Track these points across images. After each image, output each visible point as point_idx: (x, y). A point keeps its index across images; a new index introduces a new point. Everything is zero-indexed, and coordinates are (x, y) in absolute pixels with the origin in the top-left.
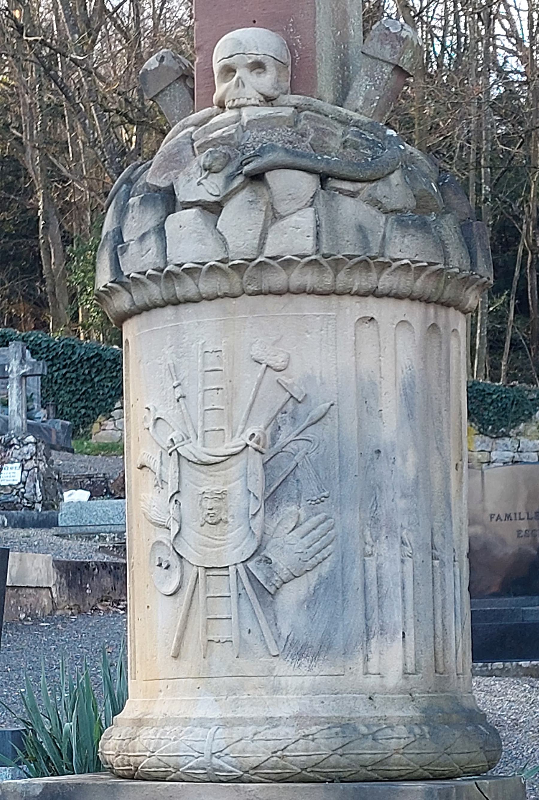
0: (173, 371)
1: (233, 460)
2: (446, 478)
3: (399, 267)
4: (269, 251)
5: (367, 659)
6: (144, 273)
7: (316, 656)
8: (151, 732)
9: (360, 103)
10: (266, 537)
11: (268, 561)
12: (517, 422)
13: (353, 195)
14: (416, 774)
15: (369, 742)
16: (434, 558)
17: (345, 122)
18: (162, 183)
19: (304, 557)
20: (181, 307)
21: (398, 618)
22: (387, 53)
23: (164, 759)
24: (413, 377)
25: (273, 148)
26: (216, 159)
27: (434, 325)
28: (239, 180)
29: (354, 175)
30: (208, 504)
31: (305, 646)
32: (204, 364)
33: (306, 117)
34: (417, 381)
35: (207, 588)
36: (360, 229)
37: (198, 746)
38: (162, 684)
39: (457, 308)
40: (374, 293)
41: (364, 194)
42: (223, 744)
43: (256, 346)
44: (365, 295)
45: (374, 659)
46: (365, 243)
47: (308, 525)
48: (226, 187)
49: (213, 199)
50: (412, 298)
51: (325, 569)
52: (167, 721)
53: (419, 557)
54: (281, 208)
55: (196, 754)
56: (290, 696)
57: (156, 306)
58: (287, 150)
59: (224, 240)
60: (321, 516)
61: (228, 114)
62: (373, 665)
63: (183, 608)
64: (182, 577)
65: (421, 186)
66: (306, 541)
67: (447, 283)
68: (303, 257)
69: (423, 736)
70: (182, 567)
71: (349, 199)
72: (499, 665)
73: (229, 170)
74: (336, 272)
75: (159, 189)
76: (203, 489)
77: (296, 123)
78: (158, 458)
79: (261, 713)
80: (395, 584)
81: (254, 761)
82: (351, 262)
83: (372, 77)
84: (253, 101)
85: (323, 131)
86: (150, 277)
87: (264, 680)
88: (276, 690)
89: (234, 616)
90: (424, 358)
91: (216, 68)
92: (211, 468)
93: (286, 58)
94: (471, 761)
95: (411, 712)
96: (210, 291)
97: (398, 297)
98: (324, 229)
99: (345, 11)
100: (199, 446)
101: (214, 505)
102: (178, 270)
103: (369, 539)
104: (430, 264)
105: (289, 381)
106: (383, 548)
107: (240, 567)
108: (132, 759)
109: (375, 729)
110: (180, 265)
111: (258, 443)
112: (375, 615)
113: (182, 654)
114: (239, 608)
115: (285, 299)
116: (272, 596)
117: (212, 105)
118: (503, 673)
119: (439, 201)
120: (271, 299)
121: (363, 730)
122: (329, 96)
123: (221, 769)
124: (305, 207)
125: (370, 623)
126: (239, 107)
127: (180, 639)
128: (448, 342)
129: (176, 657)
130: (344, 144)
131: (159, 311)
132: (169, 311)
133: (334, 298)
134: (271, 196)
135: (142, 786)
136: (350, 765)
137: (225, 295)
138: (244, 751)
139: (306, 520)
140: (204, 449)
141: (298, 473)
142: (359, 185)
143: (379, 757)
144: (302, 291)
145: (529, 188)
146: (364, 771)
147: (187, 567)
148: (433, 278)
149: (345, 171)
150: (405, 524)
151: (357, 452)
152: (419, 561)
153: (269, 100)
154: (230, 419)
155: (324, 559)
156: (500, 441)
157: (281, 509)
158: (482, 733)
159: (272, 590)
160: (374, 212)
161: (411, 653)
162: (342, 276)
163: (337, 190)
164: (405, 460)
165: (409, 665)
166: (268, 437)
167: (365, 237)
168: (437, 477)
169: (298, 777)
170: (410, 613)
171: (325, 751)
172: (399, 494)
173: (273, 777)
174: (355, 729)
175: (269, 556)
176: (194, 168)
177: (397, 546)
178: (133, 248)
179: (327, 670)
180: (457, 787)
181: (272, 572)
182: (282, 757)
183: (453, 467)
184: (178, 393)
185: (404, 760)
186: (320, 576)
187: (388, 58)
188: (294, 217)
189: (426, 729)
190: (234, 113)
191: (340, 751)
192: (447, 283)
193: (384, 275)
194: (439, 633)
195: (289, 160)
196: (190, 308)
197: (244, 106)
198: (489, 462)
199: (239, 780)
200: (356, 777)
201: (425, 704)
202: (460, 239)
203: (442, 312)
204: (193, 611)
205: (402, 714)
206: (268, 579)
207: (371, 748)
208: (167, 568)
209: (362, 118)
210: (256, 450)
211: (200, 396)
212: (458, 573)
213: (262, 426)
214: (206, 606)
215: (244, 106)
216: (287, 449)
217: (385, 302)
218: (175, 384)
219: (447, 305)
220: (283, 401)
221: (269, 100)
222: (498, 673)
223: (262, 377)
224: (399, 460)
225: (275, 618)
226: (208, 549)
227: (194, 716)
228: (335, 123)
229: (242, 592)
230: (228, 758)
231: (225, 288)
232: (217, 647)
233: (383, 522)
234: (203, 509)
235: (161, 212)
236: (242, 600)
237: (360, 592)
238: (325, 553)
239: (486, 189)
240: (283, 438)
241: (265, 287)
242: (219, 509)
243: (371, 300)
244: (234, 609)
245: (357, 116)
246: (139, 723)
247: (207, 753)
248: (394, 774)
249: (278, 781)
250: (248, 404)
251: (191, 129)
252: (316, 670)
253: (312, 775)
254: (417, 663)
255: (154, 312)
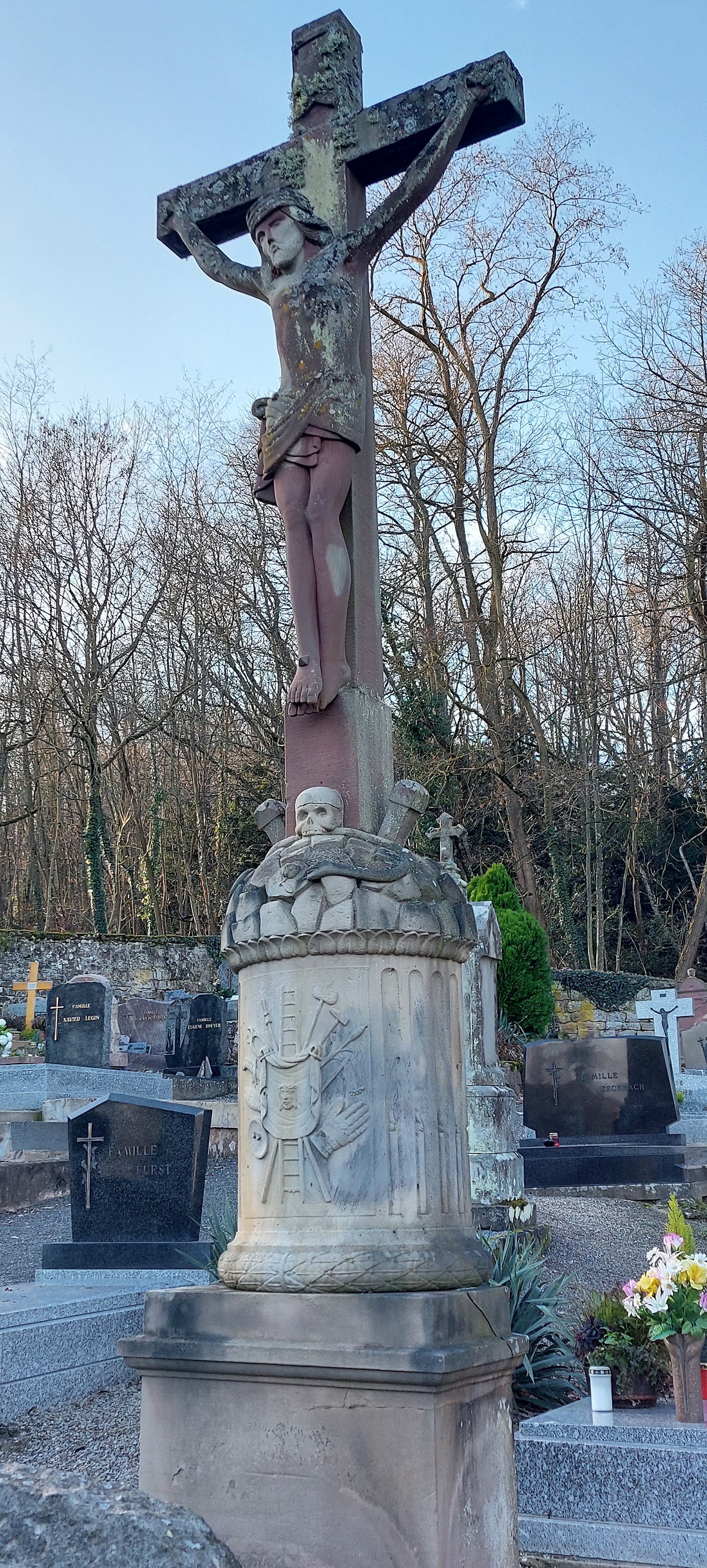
0: (264, 1005)
1: (301, 1065)
2: (449, 1074)
3: (409, 936)
4: (323, 927)
5: (391, 1204)
6: (246, 942)
7: (356, 1201)
8: (247, 1256)
9: (389, 831)
10: (323, 1118)
11: (323, 1135)
12: (623, 1000)
13: (378, 891)
14: (426, 1287)
15: (392, 1264)
16: (440, 1131)
17: (376, 844)
18: (259, 884)
19: (347, 1132)
20: (270, 963)
21: (414, 1174)
22: (404, 800)
23: (254, 1276)
24: (422, 1007)
25: (326, 863)
26: (291, 870)
27: (437, 972)
28: (305, 883)
29: (378, 879)
30: (284, 1096)
31: (349, 1195)
32: (283, 1000)
33: (351, 842)
34: (425, 1009)
35: (283, 1154)
36: (383, 912)
37: (275, 1267)
38: (255, 1221)
39: (453, 960)
40: (394, 953)
41: (385, 890)
42: (291, 1265)
43: (316, 989)
44: (388, 954)
45: (397, 1203)
46: (386, 922)
47: (350, 1110)
48: (297, 887)
49: (289, 895)
50: (419, 955)
51: (362, 1140)
52: (257, 1248)
53: (428, 1131)
54: (332, 900)
55: (274, 1273)
56: (338, 1231)
57: (255, 963)
58: (334, 864)
59: (295, 921)
60: (359, 1104)
61: (304, 840)
62: (396, 1209)
63: (269, 1168)
64: (268, 1146)
65: (425, 883)
66: (349, 1121)
67: (444, 945)
68: (345, 931)
69: (430, 1259)
70: (268, 1139)
71: (376, 894)
72: (585, 1188)
73: (299, 876)
74: (368, 940)
75: (258, 888)
76: (281, 1085)
77: (344, 847)
78: (254, 1063)
79: (318, 1243)
80: (411, 1151)
81: (312, 1278)
82: (377, 934)
83: (395, 815)
84: (318, 832)
85: (361, 851)
86: (250, 944)
87: (321, 1219)
88: (329, 1226)
89: (301, 1174)
90: (430, 995)
91: (297, 811)
92: (290, 1070)
93: (340, 805)
94: (467, 1277)
95: (423, 1241)
96: (287, 953)
97: (410, 955)
98: (358, 913)
99: (381, 774)
100: (279, 1055)
101: (288, 1096)
102: (267, 940)
103: (392, 1119)
104: (430, 933)
105: (338, 1012)
106: (402, 1124)
107: (305, 1139)
108: (234, 1276)
109: (396, 1254)
110: (268, 937)
111: (317, 1053)
112: (397, 1173)
113: (268, 1200)
114: (304, 1169)
115: (335, 957)
116: (327, 1159)
117: (295, 834)
118: (588, 1194)
119: (438, 893)
120: (326, 957)
121: (388, 1255)
122: (368, 827)
123: (290, 1283)
124: (347, 899)
125: (393, 1178)
126: (310, 836)
127: (267, 1190)
128: (448, 983)
129: (264, 1202)
130: (375, 859)
131: (257, 965)
132: (263, 965)
133: (367, 956)
134: (325, 892)
135: (237, 1295)
136: (377, 1281)
137: (297, 956)
138: (305, 1270)
139: (350, 1106)
140: (283, 1058)
141: (344, 1074)
142: (382, 885)
143: (399, 1275)
144: (346, 952)
145: (631, 833)
146: (388, 1285)
147: (271, 1139)
148: (434, 942)
149: (372, 877)
150: (419, 1108)
151: (383, 1059)
152: (429, 1134)
153: (329, 831)
154: (299, 1036)
155: (361, 1133)
156: (612, 1014)
157: (332, 1098)
158: (476, 1256)
159: (326, 1155)
160: (392, 901)
161: (423, 1198)
162: (371, 942)
163: (367, 888)
164: (418, 1064)
165: (422, 1208)
166: (324, 1050)
167: (386, 918)
168: (442, 1075)
169: (342, 1289)
170: (422, 1171)
171: (360, 1271)
172: (413, 1087)
173: (326, 1289)
174: (382, 1254)
175: (324, 1131)
176: (278, 875)
177: (413, 1123)
178: (240, 926)
179: (364, 1212)
180: (449, 1297)
181: (326, 1143)
182: (331, 1275)
183: (454, 1067)
184: (267, 1020)
185: (417, 1276)
186: (358, 1145)
187: (405, 803)
188: (339, 906)
189: (433, 1254)
190: (307, 839)
191: (371, 1271)
192: (444, 945)
193: (400, 941)
194: (444, 1184)
195: (335, 870)
196: (276, 964)
197: (313, 835)
198: (605, 1030)
199: (302, 1291)
200: (384, 1289)
201: (434, 1235)
202: (452, 916)
203: (443, 963)
204: (275, 1170)
205: (416, 1243)
206: (323, 1148)
207: (394, 1268)
208: (259, 1139)
209: (389, 842)
210: (315, 1058)
211: (280, 1022)
212: (459, 1141)
213: (320, 1042)
214: (283, 1167)
215: (313, 835)
216: (336, 1057)
217: (401, 958)
218: (265, 1013)
219: (446, 958)
220: (334, 1025)
221: (329, 831)
222: (584, 1194)
223: (320, 1009)
224: (413, 1064)
225: (329, 1174)
226: (285, 1127)
227: (274, 1245)
228: (371, 845)
229: (306, 1156)
230: (295, 1275)
231: (297, 951)
232: (290, 1195)
233: (402, 1107)
234: (281, 1099)
235: (258, 903)
236: (307, 1162)
237: (386, 1156)
238: (362, 1129)
239: (598, 835)
240: (334, 1050)
241: (322, 950)
242: (292, 1099)
243: (392, 957)
244: (301, 1169)
245: (384, 840)
246: (240, 1249)
247: (281, 1272)
248: (410, 1287)
249: (330, 1292)
250: (311, 1028)
251: (281, 849)
252: (356, 1212)
253: (352, 1288)
254: (428, 1206)
255: (254, 966)
